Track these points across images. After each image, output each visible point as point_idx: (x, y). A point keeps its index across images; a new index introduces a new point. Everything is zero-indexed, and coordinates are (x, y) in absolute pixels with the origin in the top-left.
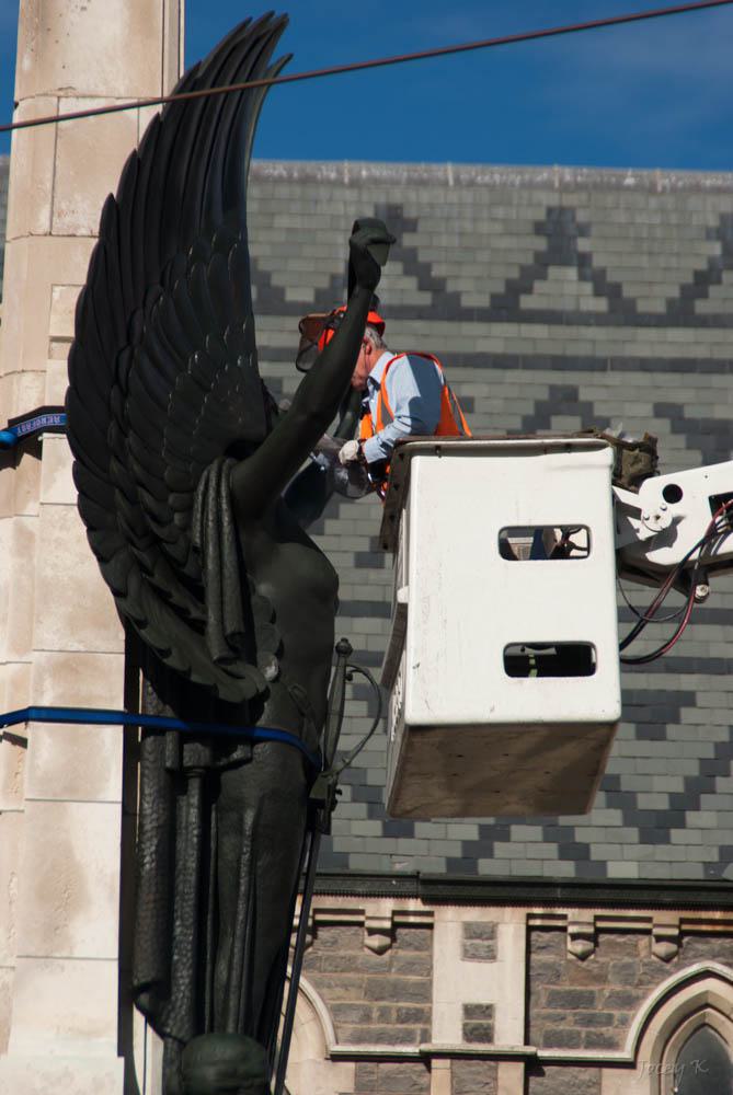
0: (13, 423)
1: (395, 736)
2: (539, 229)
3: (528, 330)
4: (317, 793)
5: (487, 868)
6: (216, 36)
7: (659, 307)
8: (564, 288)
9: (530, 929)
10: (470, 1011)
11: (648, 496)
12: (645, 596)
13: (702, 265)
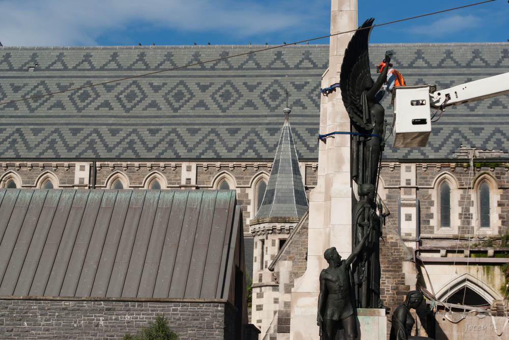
0: (331, 86)
1: (394, 135)
2: (303, 54)
3: (414, 70)
4: (382, 144)
5: (409, 157)
6: (363, 23)
7: (436, 65)
8: (420, 62)
9: (416, 167)
10: (407, 180)
11: (435, 95)
12: (435, 111)
13: (443, 58)
